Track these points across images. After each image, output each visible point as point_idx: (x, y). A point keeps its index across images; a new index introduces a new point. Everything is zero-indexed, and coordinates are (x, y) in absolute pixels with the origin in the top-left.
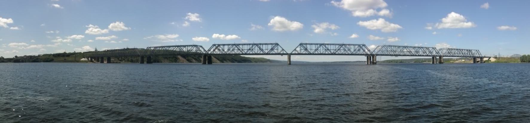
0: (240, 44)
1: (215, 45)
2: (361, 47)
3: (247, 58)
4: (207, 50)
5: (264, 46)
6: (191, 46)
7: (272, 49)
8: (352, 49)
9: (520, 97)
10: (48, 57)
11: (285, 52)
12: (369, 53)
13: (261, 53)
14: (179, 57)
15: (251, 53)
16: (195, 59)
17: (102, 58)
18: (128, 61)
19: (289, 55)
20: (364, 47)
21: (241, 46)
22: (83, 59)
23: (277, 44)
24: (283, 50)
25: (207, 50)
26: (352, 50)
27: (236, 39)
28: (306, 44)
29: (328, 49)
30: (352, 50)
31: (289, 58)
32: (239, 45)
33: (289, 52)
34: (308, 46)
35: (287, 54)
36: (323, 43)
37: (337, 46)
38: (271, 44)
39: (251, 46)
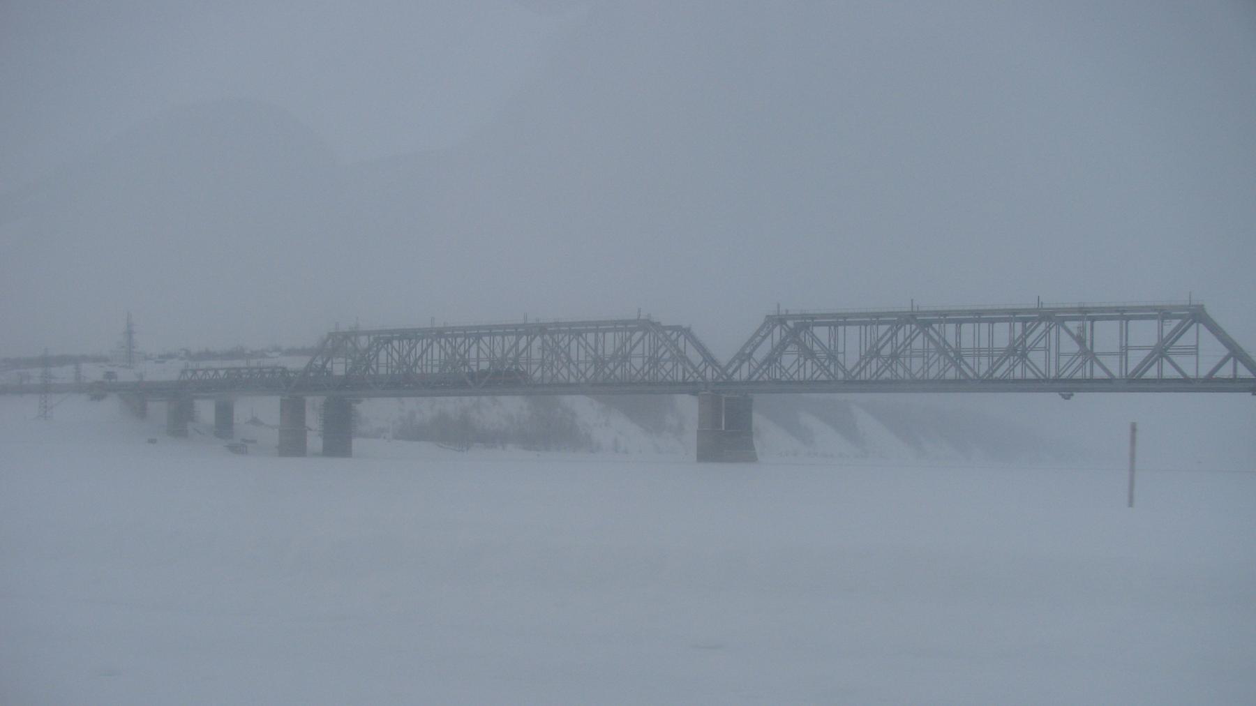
5: (967, 328)
7: (1018, 351)
23: (1197, 315)
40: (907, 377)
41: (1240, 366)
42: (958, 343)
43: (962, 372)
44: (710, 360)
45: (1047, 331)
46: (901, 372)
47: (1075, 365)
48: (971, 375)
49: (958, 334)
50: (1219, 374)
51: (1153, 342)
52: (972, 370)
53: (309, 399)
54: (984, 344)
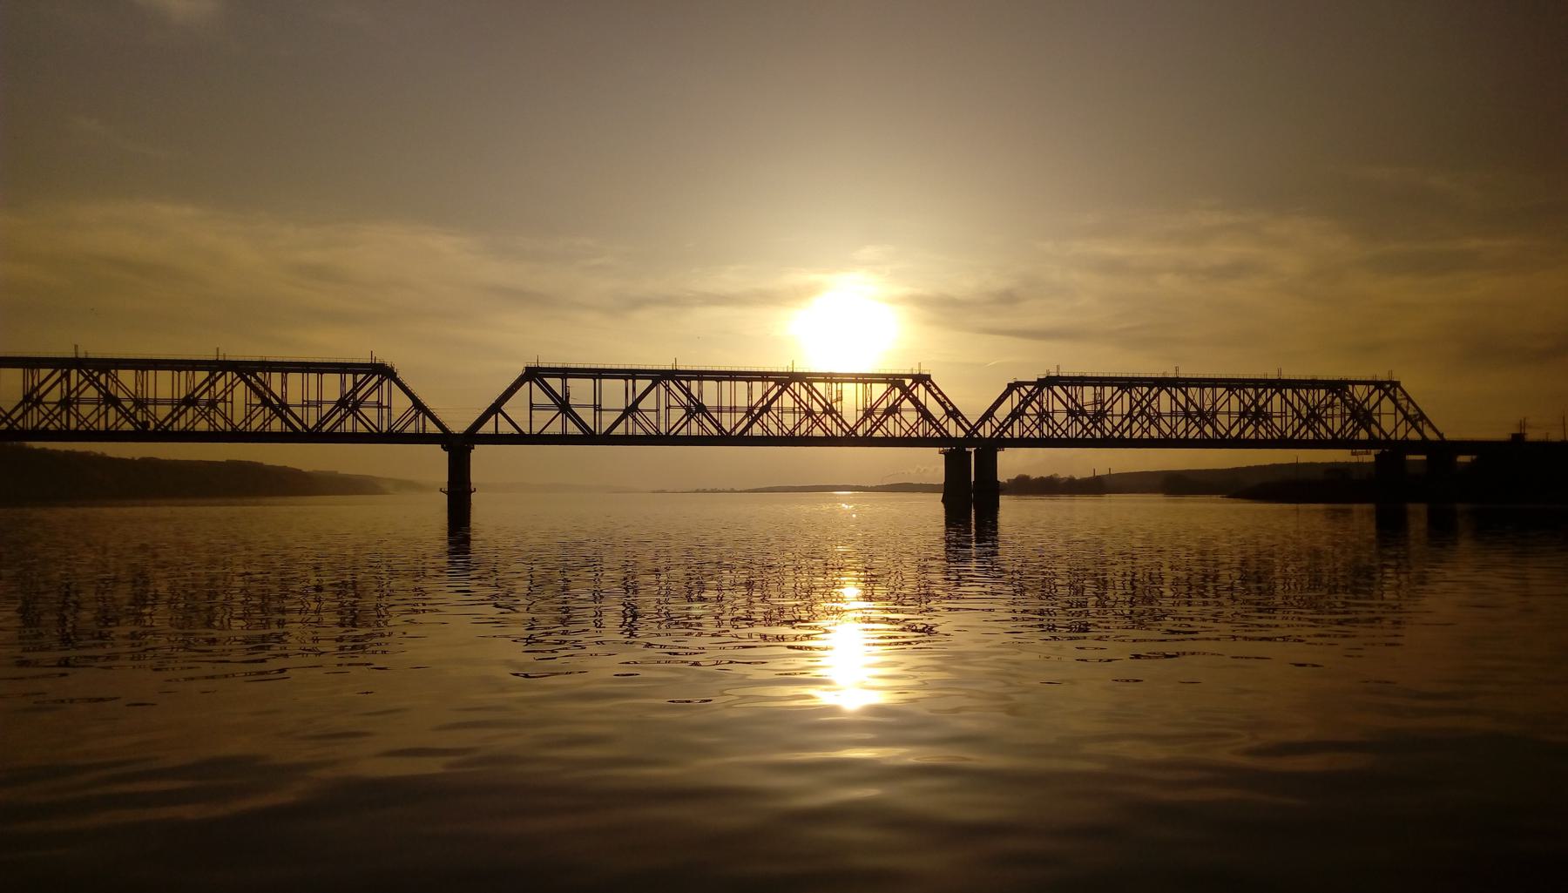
2: (906, 392)
4: (973, 412)
5: (294, 378)
7: (349, 404)
8: (851, 400)
9: (609, 674)
11: (432, 428)
12: (954, 430)
13: (277, 425)
15: (203, 426)
20: (920, 392)
21: (127, 377)
23: (385, 372)
24: (419, 406)
25: (973, 412)
28: (565, 373)
29: (701, 408)
32: (109, 365)
33: (458, 425)
34: (580, 390)
36: (666, 364)
37: (879, 389)
39: (202, 375)
40: (229, 428)
41: (570, 424)
42: (284, 394)
43: (289, 423)
44: (954, 413)
45: (380, 383)
46: (220, 422)
47: (662, 421)
48: (299, 427)
49: (284, 383)
50: (615, 432)
51: (337, 397)
52: (301, 422)
53: (1411, 507)
54: (313, 397)
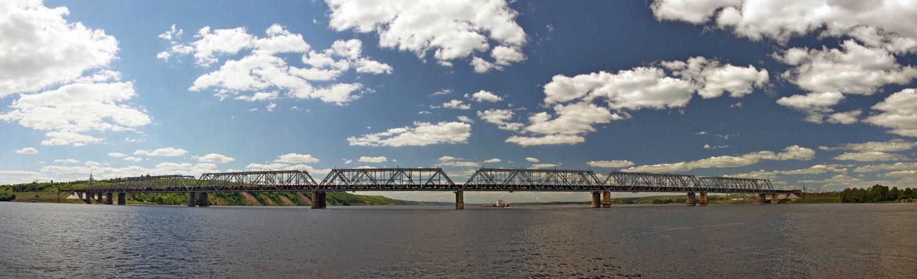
0: (345, 170)
1: (335, 171)
3: (356, 196)
6: (258, 173)
7: (392, 180)
10: (151, 182)
14: (244, 194)
16: (273, 199)
17: (110, 196)
18: (153, 201)
19: (459, 190)
22: (71, 197)
26: (570, 181)
27: (384, 163)
30: (570, 181)
31: (459, 197)
35: (452, 187)
38: (391, 170)
39: (355, 173)
